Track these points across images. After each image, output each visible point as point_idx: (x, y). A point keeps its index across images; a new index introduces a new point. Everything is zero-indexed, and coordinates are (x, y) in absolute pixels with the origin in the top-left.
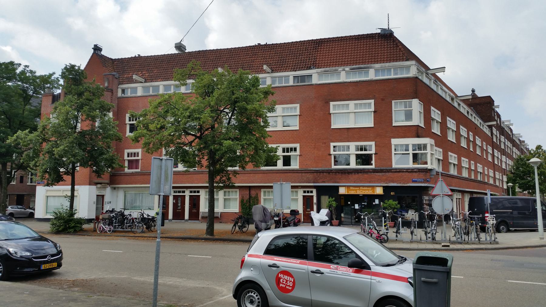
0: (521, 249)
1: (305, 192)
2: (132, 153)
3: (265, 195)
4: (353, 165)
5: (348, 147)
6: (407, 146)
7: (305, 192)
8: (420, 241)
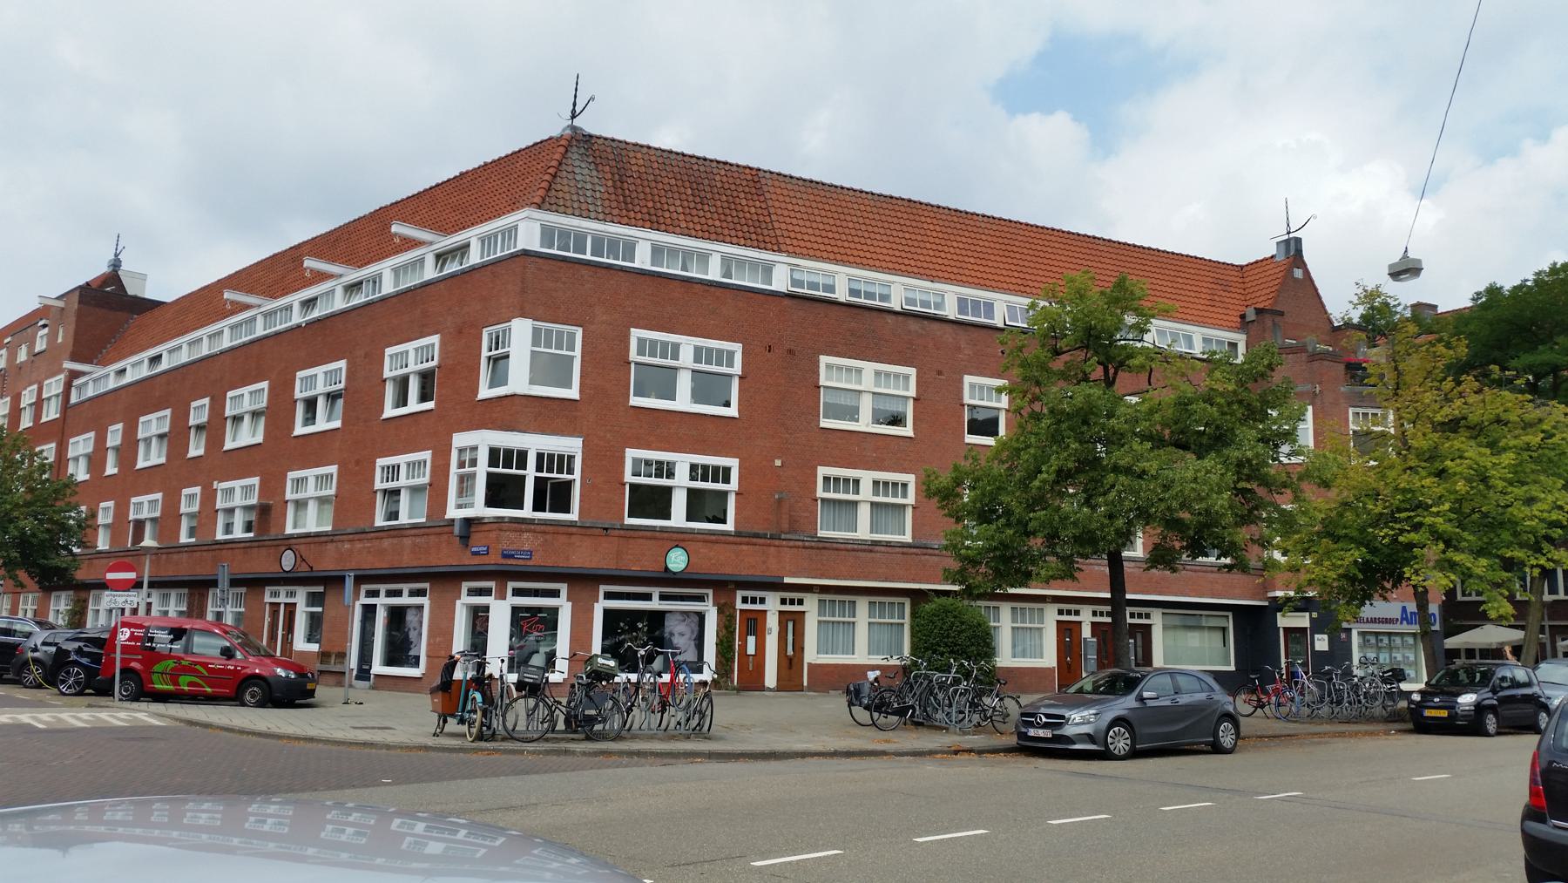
0: (812, 747)
1: (1061, 612)
4: (678, 515)
6: (523, 455)
7: (783, 602)
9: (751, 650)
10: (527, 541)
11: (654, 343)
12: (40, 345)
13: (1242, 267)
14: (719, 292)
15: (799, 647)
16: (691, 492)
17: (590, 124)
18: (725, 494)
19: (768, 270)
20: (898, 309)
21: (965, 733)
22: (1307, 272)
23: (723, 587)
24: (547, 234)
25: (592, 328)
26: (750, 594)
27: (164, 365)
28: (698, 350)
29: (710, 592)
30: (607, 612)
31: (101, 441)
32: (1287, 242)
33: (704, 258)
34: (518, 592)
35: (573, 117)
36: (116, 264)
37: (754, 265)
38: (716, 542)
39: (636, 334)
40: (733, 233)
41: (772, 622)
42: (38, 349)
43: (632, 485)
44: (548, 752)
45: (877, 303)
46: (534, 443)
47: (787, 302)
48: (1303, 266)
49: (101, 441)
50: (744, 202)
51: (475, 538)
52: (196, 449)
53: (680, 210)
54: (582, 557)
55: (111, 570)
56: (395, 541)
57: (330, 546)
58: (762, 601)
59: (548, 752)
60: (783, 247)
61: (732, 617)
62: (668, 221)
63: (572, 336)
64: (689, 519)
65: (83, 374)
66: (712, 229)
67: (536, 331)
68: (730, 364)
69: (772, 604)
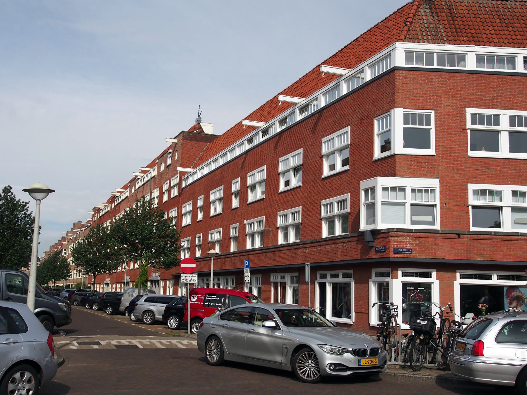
11: (482, 116)
12: (169, 162)
16: (511, 132)
25: (440, 110)
28: (512, 119)
31: (195, 204)
39: (469, 111)
42: (168, 164)
43: (471, 130)
49: (195, 204)
52: (233, 248)
53: (493, 32)
56: (333, 246)
57: (301, 250)
62: (485, 40)
64: (511, 151)
65: (186, 173)
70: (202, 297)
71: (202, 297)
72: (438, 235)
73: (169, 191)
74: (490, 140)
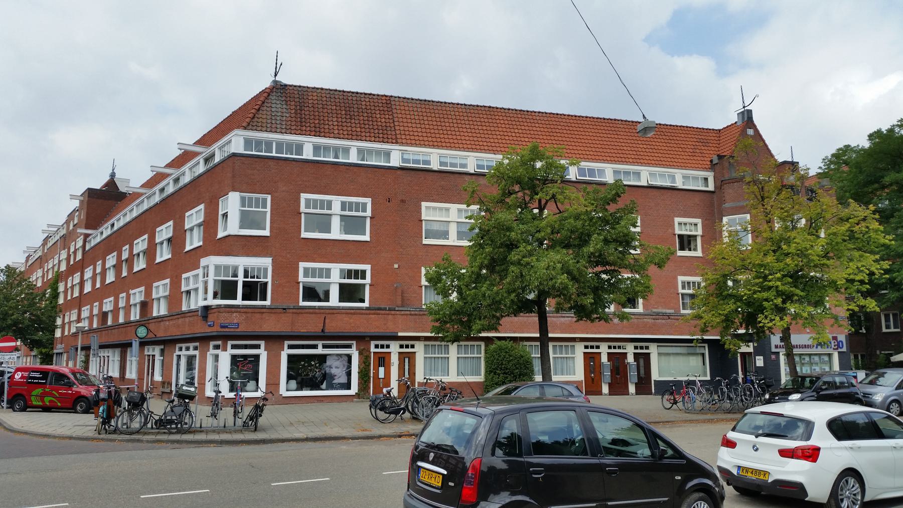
1: (586, 347)
2: (689, 283)
3: (555, 353)
4: (334, 300)
5: (328, 271)
6: (236, 269)
8: (225, 429)
9: (382, 374)
10: (235, 318)
11: (315, 201)
13: (720, 130)
14: (355, 169)
15: (412, 373)
16: (343, 217)
17: (285, 78)
18: (364, 285)
19: (387, 154)
20: (473, 172)
21: (171, 433)
22: (757, 131)
23: (362, 339)
24: (248, 143)
25: (276, 195)
26: (380, 343)
27: (116, 228)
28: (343, 204)
29: (354, 342)
30: (289, 356)
32: (743, 113)
33: (346, 150)
34: (233, 347)
35: (276, 75)
36: (113, 175)
37: (378, 153)
38: (354, 314)
40: (368, 134)
41: (395, 359)
44: (128, 441)
45: (458, 169)
46: (242, 262)
47: (399, 172)
48: (754, 126)
50: (378, 116)
51: (211, 318)
53: (336, 123)
54: (271, 325)
55: (483, 330)
57: (162, 323)
58: (388, 347)
59: (128, 441)
60: (399, 141)
61: (368, 357)
62: (327, 131)
63: (265, 200)
66: (354, 133)
67: (243, 200)
68: (364, 210)
69: (394, 348)
70: (26, 374)
71: (26, 374)
72: (264, 310)
73: (75, 252)
74: (324, 224)
